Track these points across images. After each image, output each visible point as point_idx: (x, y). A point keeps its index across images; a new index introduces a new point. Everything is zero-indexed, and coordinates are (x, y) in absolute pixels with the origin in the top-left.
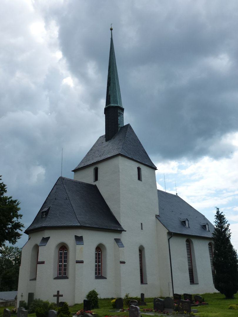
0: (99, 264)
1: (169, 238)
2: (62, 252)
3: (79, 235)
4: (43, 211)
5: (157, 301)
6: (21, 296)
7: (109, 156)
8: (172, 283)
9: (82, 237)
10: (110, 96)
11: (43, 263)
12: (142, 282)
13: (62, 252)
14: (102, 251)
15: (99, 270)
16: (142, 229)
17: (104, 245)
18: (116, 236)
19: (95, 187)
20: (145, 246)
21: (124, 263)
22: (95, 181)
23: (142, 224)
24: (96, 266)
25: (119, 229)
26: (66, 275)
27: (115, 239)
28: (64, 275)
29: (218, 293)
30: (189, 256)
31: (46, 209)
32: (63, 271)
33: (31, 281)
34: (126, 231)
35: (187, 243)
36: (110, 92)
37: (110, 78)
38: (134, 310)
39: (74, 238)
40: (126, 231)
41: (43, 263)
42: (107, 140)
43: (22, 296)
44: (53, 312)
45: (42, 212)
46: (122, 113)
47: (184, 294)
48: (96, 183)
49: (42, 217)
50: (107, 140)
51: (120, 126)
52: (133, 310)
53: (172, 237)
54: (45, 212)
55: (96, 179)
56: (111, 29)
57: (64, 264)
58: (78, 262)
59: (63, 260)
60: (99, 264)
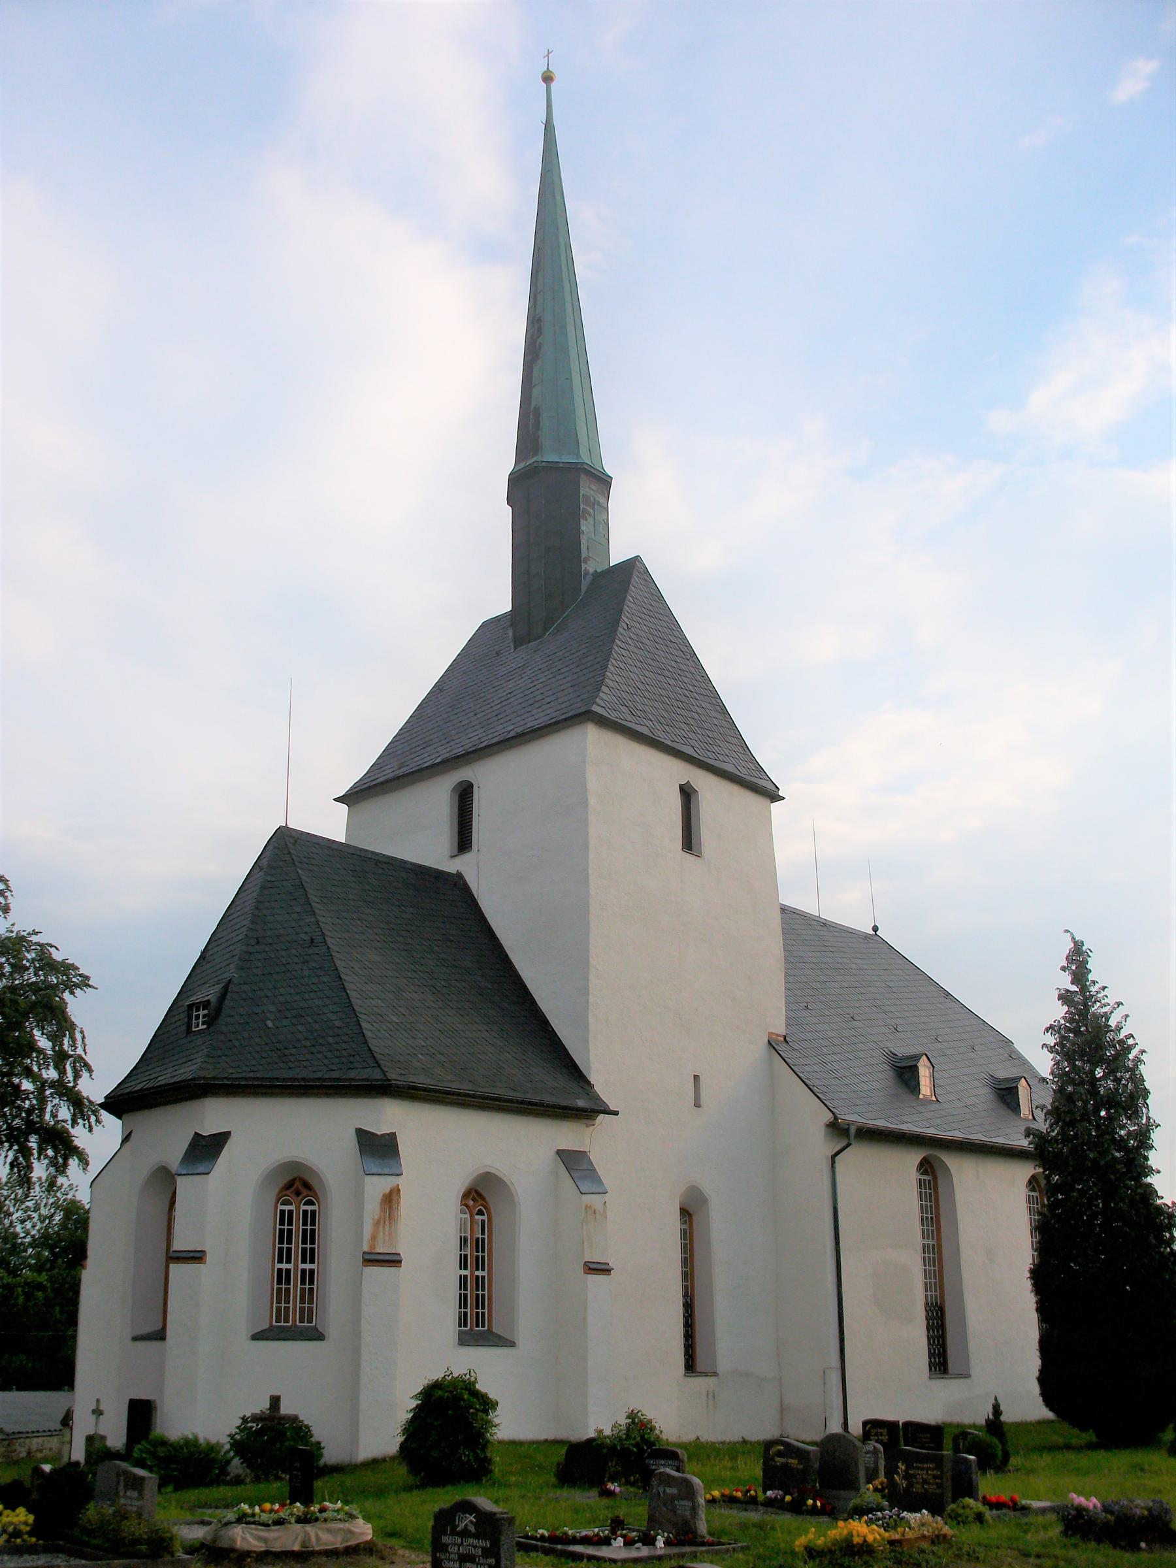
0: (477, 1273)
1: (830, 1153)
2: (292, 1208)
3: (381, 1129)
4: (194, 999)
5: (779, 1451)
6: (94, 1412)
7: (531, 723)
8: (839, 1372)
9: (392, 1137)
10: (537, 412)
11: (196, 1257)
12: (690, 1366)
13: (292, 1208)
14: (491, 1205)
15: (479, 1301)
16: (697, 1104)
17: (504, 1182)
18: (566, 1135)
19: (457, 885)
20: (709, 1190)
21: (604, 1270)
22: (456, 852)
23: (696, 1077)
24: (463, 1281)
25: (581, 1103)
26: (310, 1321)
27: (560, 1153)
28: (301, 1321)
29: (1053, 1421)
30: (931, 1242)
31: (210, 993)
32: (295, 1305)
33: (141, 1345)
34: (616, 1113)
35: (923, 1177)
36: (536, 392)
37: (539, 320)
38: (674, 1491)
39: (350, 1142)
40: (616, 1113)
41: (196, 1257)
42: (519, 642)
43: (98, 1412)
44: (966, 1458)
45: (190, 1007)
46: (602, 500)
47: (907, 1425)
48: (462, 865)
49: (189, 1031)
50: (519, 642)
51: (591, 570)
52: (668, 1490)
53: (849, 1145)
54: (206, 1005)
55: (464, 842)
56: (548, 78)
57: (302, 1266)
58: (372, 1260)
59: (297, 1246)
60: (479, 1273)
